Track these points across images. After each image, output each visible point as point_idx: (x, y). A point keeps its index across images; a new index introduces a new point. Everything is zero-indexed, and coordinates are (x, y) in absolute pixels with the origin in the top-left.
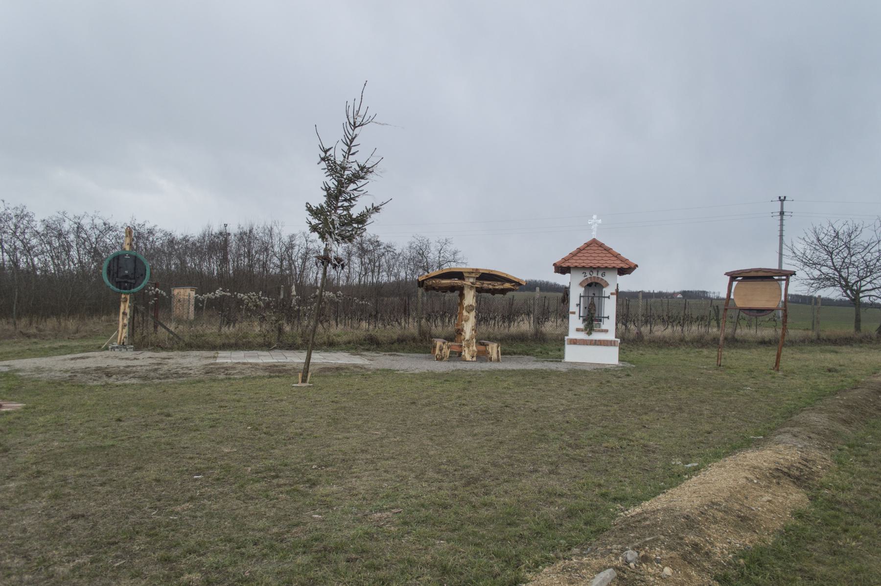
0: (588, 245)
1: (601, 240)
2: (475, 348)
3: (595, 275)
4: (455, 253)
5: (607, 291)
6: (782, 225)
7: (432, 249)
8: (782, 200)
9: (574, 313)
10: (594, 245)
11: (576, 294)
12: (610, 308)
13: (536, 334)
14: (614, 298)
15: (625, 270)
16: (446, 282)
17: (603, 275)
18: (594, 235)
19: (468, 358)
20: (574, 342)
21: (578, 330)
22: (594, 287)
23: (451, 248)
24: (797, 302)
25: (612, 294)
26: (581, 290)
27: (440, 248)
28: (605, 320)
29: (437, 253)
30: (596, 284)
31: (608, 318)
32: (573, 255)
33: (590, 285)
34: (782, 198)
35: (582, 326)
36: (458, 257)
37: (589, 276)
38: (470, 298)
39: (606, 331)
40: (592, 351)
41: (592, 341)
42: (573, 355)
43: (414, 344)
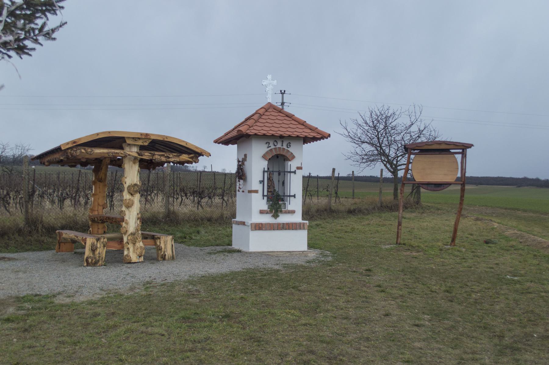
2: (141, 244)
3: (279, 145)
5: (292, 165)
8: (283, 93)
9: (256, 192)
11: (257, 167)
12: (295, 185)
16: (99, 151)
17: (289, 145)
18: (269, 101)
19: (134, 258)
20: (259, 227)
21: (262, 212)
22: (278, 161)
26: (264, 164)
28: (292, 198)
31: (294, 196)
34: (283, 92)
35: (265, 207)
37: (273, 147)
38: (132, 175)
39: (293, 212)
40: (270, 236)
41: (279, 224)
42: (258, 243)
43: (20, 239)
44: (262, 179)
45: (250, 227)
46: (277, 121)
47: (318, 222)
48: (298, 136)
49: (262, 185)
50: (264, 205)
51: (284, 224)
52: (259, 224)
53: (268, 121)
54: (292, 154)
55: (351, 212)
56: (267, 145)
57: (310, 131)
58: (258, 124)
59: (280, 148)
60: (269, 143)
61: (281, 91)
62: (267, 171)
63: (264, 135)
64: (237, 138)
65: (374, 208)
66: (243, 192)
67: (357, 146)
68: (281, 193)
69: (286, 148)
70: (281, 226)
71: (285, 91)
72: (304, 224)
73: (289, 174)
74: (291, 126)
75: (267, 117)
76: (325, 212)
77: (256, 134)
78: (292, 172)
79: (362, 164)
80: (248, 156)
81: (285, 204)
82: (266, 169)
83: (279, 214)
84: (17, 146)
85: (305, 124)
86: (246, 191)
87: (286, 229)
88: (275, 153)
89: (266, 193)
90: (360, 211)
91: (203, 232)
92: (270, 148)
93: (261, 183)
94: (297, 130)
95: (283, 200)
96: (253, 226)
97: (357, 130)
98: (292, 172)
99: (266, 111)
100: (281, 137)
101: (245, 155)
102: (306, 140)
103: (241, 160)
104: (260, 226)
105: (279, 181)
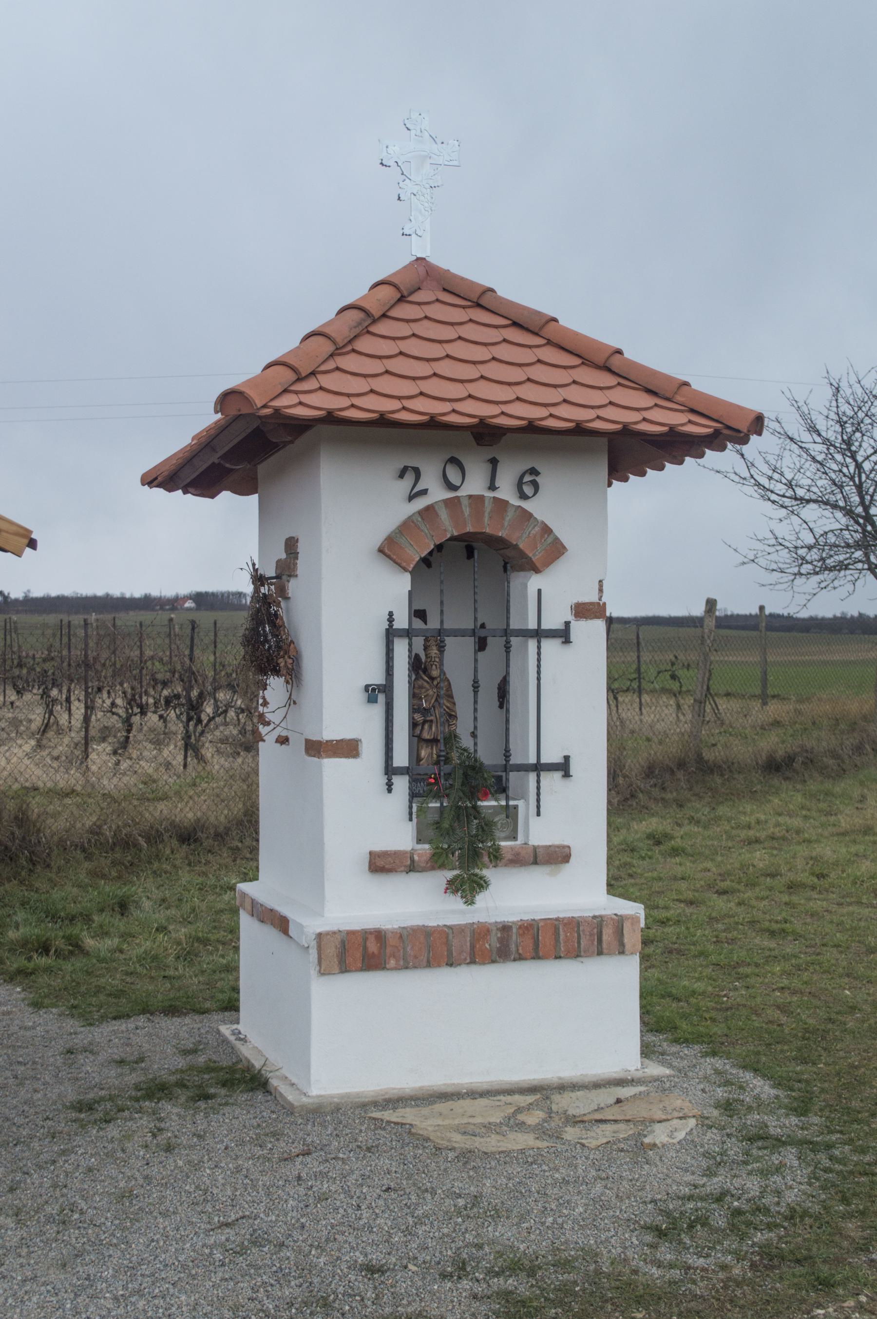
3: (474, 484)
5: (550, 594)
9: (348, 749)
10: (420, 288)
11: (352, 611)
12: (570, 706)
14: (591, 636)
17: (529, 484)
20: (363, 952)
21: (381, 864)
22: (469, 568)
25: (583, 611)
28: (551, 781)
30: (497, 544)
31: (564, 767)
35: (401, 836)
37: (437, 494)
39: (557, 856)
41: (479, 932)
42: (344, 1043)
44: (378, 678)
45: (313, 954)
46: (460, 350)
48: (579, 430)
49: (377, 711)
50: (389, 820)
51: (505, 928)
52: (365, 934)
53: (413, 347)
54: (547, 530)
55: (777, 767)
57: (646, 401)
58: (349, 362)
62: (408, 633)
63: (383, 421)
64: (244, 449)
65: (859, 749)
66: (283, 741)
67: (783, 512)
68: (488, 756)
69: (515, 501)
70: (493, 942)
72: (619, 923)
73: (532, 644)
74: (540, 373)
75: (404, 330)
76: (680, 775)
77: (331, 418)
78: (552, 634)
79: (799, 581)
80: (301, 548)
81: (511, 813)
82: (402, 622)
83: (487, 873)
86: (297, 744)
87: (520, 958)
88: (448, 528)
89: (401, 758)
90: (811, 761)
91: (146, 908)
92: (420, 503)
93: (372, 700)
94: (575, 394)
95: (501, 788)
96: (331, 951)
97: (780, 457)
98: (552, 634)
99: (402, 299)
100: (486, 435)
101: (291, 545)
102: (630, 452)
103: (270, 571)
105: (476, 686)
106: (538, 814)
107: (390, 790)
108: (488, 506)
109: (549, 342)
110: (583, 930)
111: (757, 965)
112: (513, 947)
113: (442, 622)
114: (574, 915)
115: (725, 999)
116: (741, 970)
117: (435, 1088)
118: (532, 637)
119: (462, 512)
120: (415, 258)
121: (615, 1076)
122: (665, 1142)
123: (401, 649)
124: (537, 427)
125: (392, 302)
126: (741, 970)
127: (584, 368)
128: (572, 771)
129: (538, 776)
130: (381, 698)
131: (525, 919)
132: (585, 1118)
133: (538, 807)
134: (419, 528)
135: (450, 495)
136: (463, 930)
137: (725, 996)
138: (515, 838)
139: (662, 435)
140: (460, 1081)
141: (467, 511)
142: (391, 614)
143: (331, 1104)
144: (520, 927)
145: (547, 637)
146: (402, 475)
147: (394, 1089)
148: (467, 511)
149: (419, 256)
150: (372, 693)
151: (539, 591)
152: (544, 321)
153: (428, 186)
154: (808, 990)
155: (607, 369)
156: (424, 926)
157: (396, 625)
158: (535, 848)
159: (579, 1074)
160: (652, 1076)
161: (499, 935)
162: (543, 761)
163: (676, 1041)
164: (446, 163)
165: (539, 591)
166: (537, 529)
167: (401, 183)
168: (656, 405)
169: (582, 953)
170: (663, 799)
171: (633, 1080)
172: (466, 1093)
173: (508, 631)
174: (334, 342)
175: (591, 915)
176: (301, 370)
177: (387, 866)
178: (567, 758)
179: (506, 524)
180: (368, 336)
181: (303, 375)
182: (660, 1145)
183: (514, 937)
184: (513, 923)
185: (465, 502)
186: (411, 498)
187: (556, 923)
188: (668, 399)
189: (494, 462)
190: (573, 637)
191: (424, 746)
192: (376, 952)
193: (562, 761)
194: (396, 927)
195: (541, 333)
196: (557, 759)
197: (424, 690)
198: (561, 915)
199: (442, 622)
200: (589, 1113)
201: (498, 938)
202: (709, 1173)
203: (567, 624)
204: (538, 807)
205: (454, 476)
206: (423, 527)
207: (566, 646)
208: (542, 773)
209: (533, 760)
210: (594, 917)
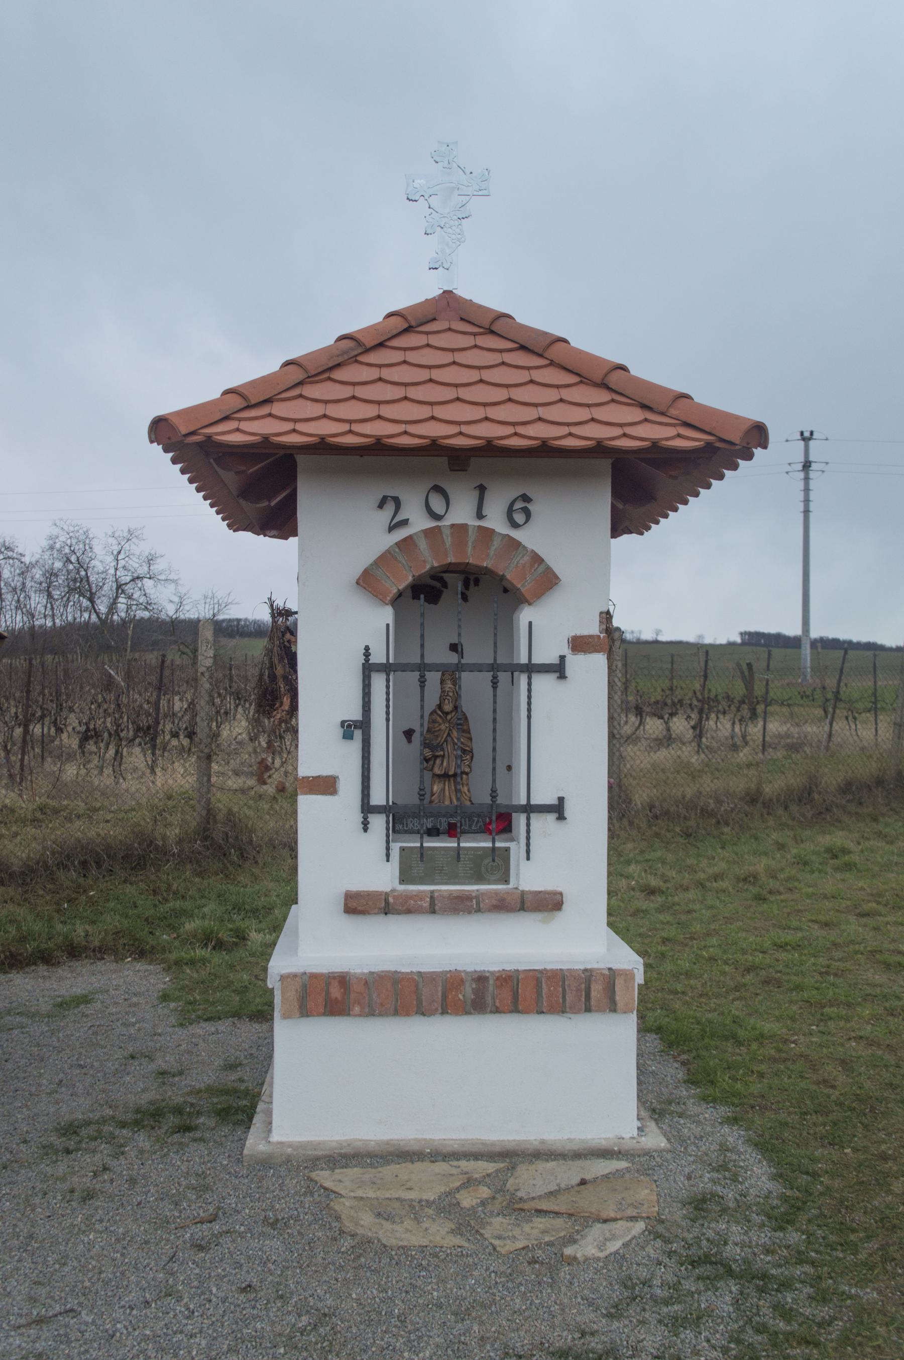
0: (409, 323)
1: (485, 292)
3: (461, 513)
4: (150, 561)
5: (546, 627)
6: (807, 490)
7: (98, 549)
8: (806, 438)
9: (326, 785)
11: (341, 653)
12: (565, 742)
13: (204, 832)
14: (592, 672)
15: (656, 467)
17: (520, 512)
20: (333, 996)
21: (357, 905)
22: (455, 598)
23: (140, 548)
24: (758, 645)
25: (580, 644)
26: (371, 625)
27: (116, 549)
28: (542, 824)
29: (110, 559)
31: (558, 809)
32: (306, 374)
33: (427, 591)
34: (807, 434)
35: (382, 877)
36: (156, 567)
37: (419, 523)
39: (549, 903)
47: (837, 838)
49: (355, 746)
54: (537, 559)
56: (386, 515)
59: (460, 529)
60: (397, 502)
61: (802, 433)
70: (468, 990)
71: (812, 433)
72: (611, 978)
78: (545, 669)
84: (206, 597)
85: (615, 379)
87: (497, 1011)
88: (429, 561)
92: (401, 534)
93: (348, 736)
98: (545, 669)
104: (336, 992)
106: (528, 859)
107: (365, 829)
108: (472, 535)
109: (552, 363)
110: (569, 985)
111: (849, 1005)
112: (489, 999)
113: (422, 656)
114: (563, 968)
115: (793, 1045)
116: (827, 1010)
117: (402, 1143)
118: (522, 671)
119: (443, 541)
120: (441, 291)
121: (604, 1144)
122: (590, 1255)
123: (378, 682)
124: (498, 447)
125: (395, 332)
126: (827, 1010)
127: (582, 388)
128: (567, 814)
129: (528, 819)
130: (358, 734)
131: (508, 969)
132: (526, 1206)
133: (528, 852)
134: (396, 559)
135: (432, 524)
136: (434, 979)
137: (793, 1042)
138: (507, 882)
139: (639, 451)
140: (432, 1137)
141: (448, 541)
142: (367, 648)
143: (282, 1155)
144: (498, 978)
145: (539, 672)
146: (381, 506)
147: (361, 1140)
148: (448, 541)
149: (446, 288)
150: (348, 729)
151: (530, 623)
152: (548, 341)
153: (456, 218)
154: (887, 1042)
155: (603, 385)
156: (396, 972)
157: (373, 660)
158: (523, 892)
159: (566, 1138)
160: (643, 1149)
161: (474, 986)
162: (532, 802)
163: (704, 1099)
164: (475, 193)
165: (530, 623)
166: (526, 558)
167: (428, 217)
168: (646, 420)
169: (568, 1010)
170: (857, 813)
171: (620, 1152)
172: (429, 1153)
173: (495, 666)
174: (306, 371)
175: (582, 967)
176: (250, 397)
177: (359, 908)
178: (561, 800)
179: (492, 553)
180: (356, 365)
181: (253, 402)
182: (581, 1259)
183: (491, 989)
184: (492, 973)
185: (446, 533)
186: (391, 529)
187: (539, 975)
188: (662, 414)
189: (482, 489)
190: (569, 671)
191: (437, 781)
192: (339, 997)
193: (555, 802)
194: (366, 971)
195: (546, 355)
196: (551, 800)
197: (437, 725)
198: (549, 967)
199: (422, 656)
200: (540, 1197)
201: (473, 989)
202: (615, 1313)
203: (562, 658)
204: (528, 852)
205: (438, 505)
206: (400, 558)
207: (562, 681)
208: (532, 815)
209: (523, 802)
210: (586, 970)
